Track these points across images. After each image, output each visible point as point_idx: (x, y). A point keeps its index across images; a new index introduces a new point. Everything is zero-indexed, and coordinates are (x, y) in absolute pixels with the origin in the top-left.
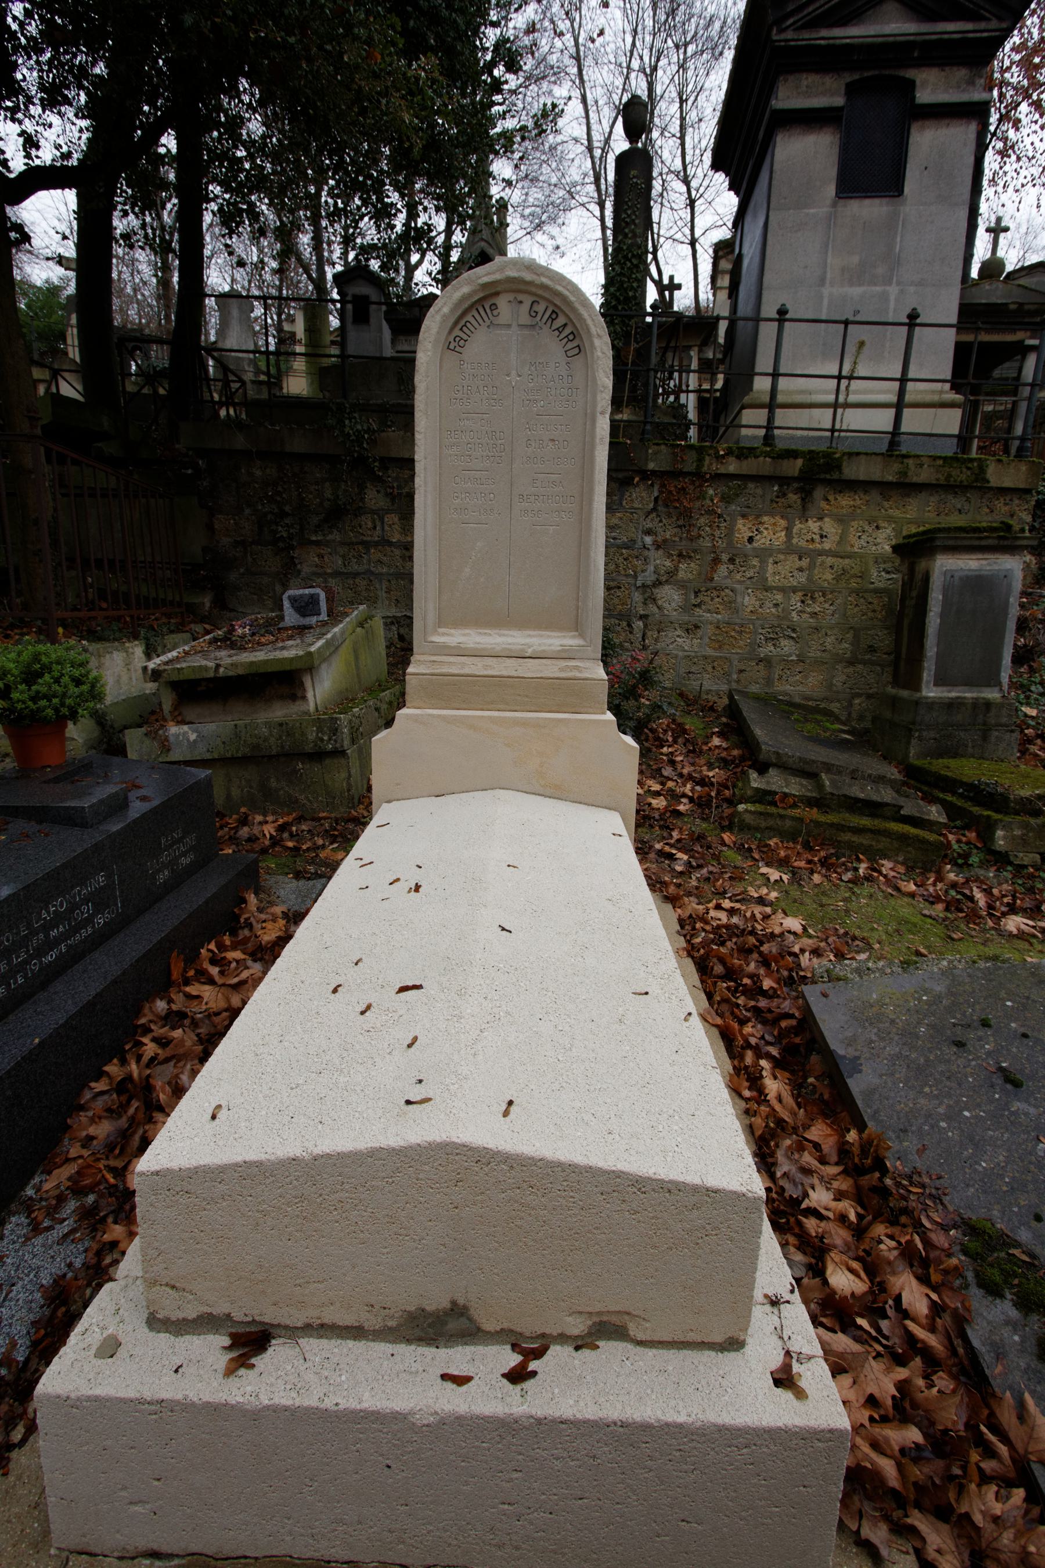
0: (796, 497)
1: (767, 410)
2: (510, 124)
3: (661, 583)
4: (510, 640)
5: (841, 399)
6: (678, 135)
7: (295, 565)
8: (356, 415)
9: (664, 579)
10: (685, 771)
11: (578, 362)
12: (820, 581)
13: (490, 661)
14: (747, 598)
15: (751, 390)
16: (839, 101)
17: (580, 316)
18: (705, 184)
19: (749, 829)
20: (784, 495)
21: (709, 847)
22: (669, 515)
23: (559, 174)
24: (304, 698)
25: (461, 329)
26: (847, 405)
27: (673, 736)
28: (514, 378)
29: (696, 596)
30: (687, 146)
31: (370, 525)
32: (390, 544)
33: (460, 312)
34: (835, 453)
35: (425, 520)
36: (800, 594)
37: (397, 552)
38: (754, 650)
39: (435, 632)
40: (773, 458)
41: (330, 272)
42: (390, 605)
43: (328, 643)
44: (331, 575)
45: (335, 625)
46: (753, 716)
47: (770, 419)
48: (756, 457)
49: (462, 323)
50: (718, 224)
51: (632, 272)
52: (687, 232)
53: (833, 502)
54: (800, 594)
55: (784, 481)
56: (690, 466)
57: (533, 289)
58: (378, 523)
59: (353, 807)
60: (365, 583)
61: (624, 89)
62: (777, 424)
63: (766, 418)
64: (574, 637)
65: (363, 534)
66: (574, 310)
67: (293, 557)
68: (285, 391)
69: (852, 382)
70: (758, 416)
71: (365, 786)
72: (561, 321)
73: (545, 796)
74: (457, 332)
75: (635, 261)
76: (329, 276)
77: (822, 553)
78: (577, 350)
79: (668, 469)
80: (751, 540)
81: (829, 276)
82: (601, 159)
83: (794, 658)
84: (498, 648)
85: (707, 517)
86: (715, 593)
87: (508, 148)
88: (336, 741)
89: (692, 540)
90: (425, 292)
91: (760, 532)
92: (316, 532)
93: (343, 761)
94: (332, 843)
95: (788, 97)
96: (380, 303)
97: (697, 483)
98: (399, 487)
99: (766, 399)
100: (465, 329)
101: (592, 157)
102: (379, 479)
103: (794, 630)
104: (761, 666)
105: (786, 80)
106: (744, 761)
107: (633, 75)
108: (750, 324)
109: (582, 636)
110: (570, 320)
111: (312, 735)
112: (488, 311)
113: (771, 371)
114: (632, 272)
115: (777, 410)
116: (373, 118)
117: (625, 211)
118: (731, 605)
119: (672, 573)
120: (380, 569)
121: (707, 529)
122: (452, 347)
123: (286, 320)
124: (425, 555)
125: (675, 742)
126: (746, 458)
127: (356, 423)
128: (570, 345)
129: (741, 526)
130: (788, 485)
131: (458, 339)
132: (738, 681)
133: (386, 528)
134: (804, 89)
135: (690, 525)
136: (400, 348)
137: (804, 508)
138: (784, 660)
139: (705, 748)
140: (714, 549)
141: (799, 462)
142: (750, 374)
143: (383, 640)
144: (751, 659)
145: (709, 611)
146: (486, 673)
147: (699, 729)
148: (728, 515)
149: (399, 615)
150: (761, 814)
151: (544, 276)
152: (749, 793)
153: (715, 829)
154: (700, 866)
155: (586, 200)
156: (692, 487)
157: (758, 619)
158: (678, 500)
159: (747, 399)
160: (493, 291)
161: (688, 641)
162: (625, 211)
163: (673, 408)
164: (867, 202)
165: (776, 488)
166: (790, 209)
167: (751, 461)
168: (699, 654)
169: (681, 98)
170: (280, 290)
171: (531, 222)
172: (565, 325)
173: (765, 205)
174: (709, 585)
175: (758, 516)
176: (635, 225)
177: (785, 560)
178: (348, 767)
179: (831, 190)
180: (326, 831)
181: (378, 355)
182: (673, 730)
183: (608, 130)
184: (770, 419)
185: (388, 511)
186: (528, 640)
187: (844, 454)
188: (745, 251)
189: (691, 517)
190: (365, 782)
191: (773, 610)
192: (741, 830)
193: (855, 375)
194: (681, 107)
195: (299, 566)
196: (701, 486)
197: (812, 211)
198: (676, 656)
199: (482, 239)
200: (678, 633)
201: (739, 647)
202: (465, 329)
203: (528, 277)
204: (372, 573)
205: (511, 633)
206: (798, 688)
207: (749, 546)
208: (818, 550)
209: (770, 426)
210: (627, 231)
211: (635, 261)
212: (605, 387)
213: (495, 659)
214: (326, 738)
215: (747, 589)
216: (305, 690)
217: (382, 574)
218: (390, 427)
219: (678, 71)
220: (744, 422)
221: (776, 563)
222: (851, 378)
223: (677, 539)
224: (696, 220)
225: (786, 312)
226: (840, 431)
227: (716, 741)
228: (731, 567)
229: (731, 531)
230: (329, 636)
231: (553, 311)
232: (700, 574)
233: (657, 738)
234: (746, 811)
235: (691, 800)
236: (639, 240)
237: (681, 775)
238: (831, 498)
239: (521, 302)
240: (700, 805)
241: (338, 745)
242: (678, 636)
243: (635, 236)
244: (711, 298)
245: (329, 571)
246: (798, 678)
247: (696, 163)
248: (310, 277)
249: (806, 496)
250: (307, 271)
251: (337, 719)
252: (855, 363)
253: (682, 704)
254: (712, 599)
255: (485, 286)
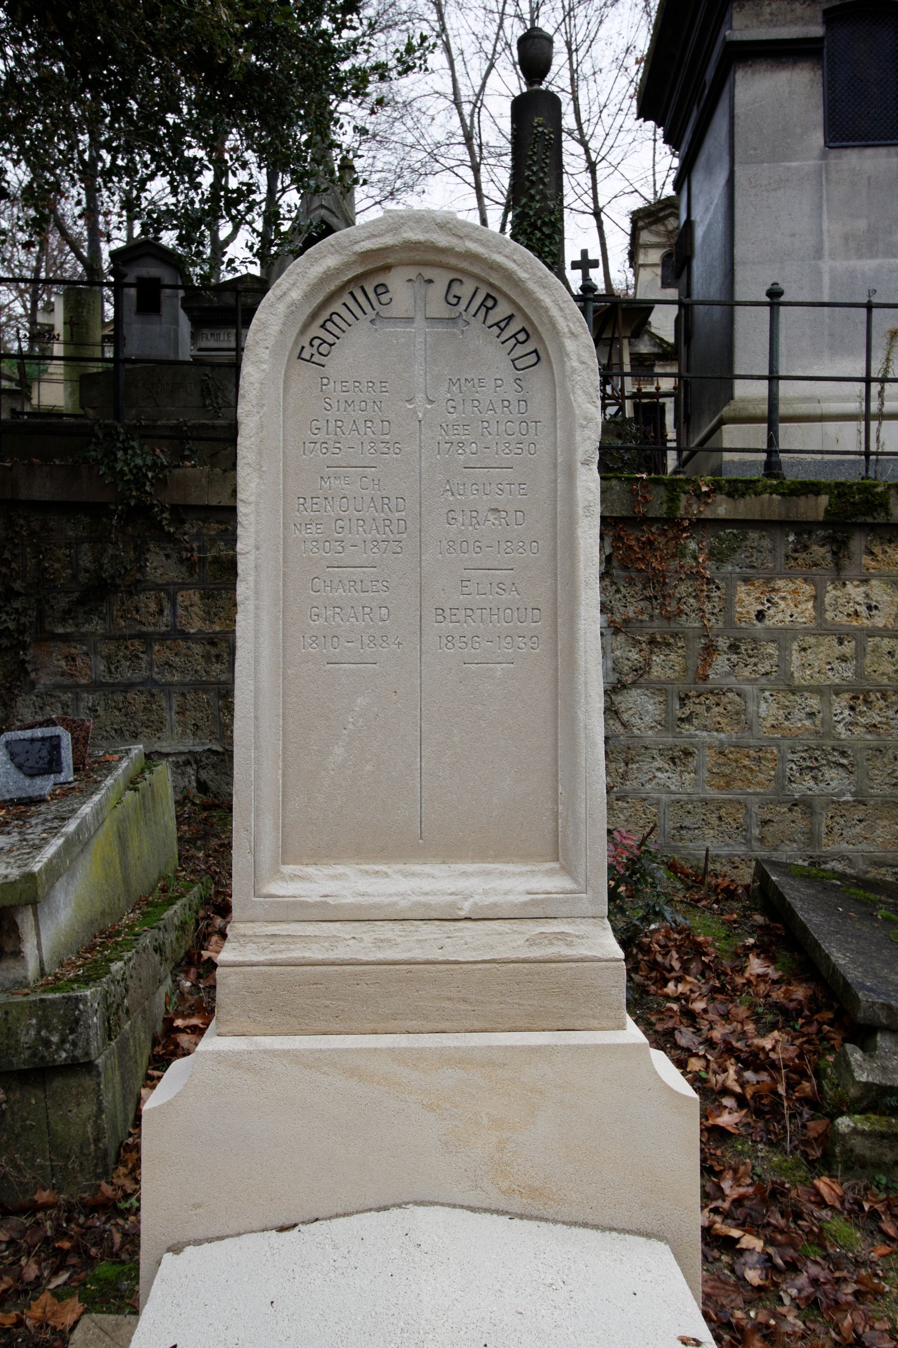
0: (823, 550)
1: (766, 425)
2: (360, 60)
3: (624, 687)
4: (426, 885)
5: (874, 407)
6: (569, 90)
7: (27, 673)
8: (135, 444)
9: (629, 679)
10: (717, 1034)
11: (536, 378)
12: (875, 676)
13: (388, 930)
14: (763, 705)
15: (732, 397)
16: (817, 30)
17: (537, 303)
18: (609, 142)
19: (863, 1166)
20: (806, 548)
21: (798, 1215)
22: (631, 583)
23: (417, 134)
24: (17, 954)
25: (323, 326)
26: (882, 417)
27: (680, 959)
28: (420, 405)
29: (683, 705)
30: (581, 101)
31: (153, 607)
32: (186, 636)
33: (320, 298)
34: (876, 486)
35: (257, 661)
36: (847, 696)
37: (197, 649)
38: (783, 788)
39: (276, 874)
40: (783, 495)
41: (106, 249)
42: (184, 733)
43: (69, 843)
44: (87, 688)
45: (86, 794)
46: (817, 920)
47: (772, 439)
48: (757, 494)
49: (325, 315)
50: (626, 191)
51: (544, 245)
52: (588, 200)
53: (881, 557)
54: (847, 696)
55: (803, 528)
56: (657, 507)
57: (453, 261)
58: (167, 605)
59: (106, 1174)
60: (143, 698)
61: (497, 39)
62: (782, 446)
63: (765, 439)
64: (550, 873)
65: (141, 622)
66: (527, 293)
67: (23, 662)
68: (35, 402)
69: (887, 386)
70: (757, 435)
71: (131, 1116)
72: (502, 310)
73: (513, 1216)
74: (315, 330)
75: (547, 230)
76: (105, 256)
77: (872, 633)
78: (533, 359)
79: (625, 513)
80: (760, 615)
81: (827, 245)
82: (472, 116)
83: (848, 798)
84: (403, 903)
85: (689, 583)
86: (712, 699)
87: (360, 92)
88: (74, 1044)
89: (669, 619)
90: (244, 272)
91: (775, 604)
92: (63, 621)
93: (88, 1082)
94: (55, 1273)
95: (747, 27)
96: (175, 287)
97: (671, 534)
98: (201, 549)
99: (764, 408)
100: (329, 325)
101: (461, 114)
102: (170, 537)
103: (843, 754)
104: (797, 814)
105: (742, 7)
106: (818, 1011)
107: (507, 22)
108: (717, 310)
109: (568, 870)
110: (519, 309)
111: (27, 1037)
112: (372, 296)
113: (766, 373)
114: (544, 245)
115: (781, 426)
116: (168, 22)
117: (529, 168)
118: (738, 716)
119: (642, 670)
120: (169, 677)
121: (692, 601)
122: (306, 355)
123: (43, 309)
124: (257, 727)
125: (686, 969)
126: (743, 495)
127: (135, 455)
128: (520, 350)
129: (743, 596)
130: (810, 533)
131: (317, 342)
132: (762, 840)
133: (180, 611)
134: (768, 17)
135: (664, 597)
136: (204, 344)
137: (838, 567)
138: (833, 802)
139: (740, 980)
140: (705, 632)
141: (824, 500)
142: (728, 378)
143: (170, 791)
144: (781, 803)
145: (705, 728)
146: (380, 956)
147: (718, 939)
148: (722, 580)
149: (199, 749)
150: (882, 1136)
151: (471, 239)
152: (853, 1092)
153: (797, 1167)
154: (793, 1267)
155: (453, 163)
156: (662, 540)
157: (784, 737)
158: (643, 559)
159: (726, 411)
160: (380, 264)
161: (675, 777)
162: (529, 168)
163: (616, 423)
164: (869, 152)
165: (791, 538)
166: (763, 162)
167: (750, 499)
168: (694, 797)
169: (569, 49)
170: (37, 270)
171: (381, 190)
172: (510, 318)
173: (726, 159)
174: (702, 686)
175: (768, 581)
176: (544, 184)
177: (818, 645)
178: (98, 1093)
179: (818, 138)
180: (47, 1240)
181: (172, 357)
182: (679, 949)
183: (480, 82)
184: (772, 439)
185: (184, 586)
186: (462, 884)
187: (890, 487)
188: (696, 216)
189: (665, 584)
190: (131, 1107)
191: (807, 723)
192: (848, 1169)
193: (890, 376)
194: (570, 59)
195: (33, 675)
196: (677, 537)
197: (794, 164)
198: (658, 803)
199: (322, 206)
200: (656, 764)
201: (758, 783)
202: (329, 325)
203: (443, 240)
204: (156, 683)
205: (427, 869)
206: (859, 847)
207: (759, 625)
208: (867, 629)
209: (772, 449)
210: (532, 192)
211: (547, 230)
212: (589, 419)
213: (397, 926)
214: (55, 1039)
215: (763, 690)
216: (19, 939)
217: (171, 684)
218: (188, 458)
219: (564, 20)
220: (726, 444)
221: (804, 649)
222: (883, 380)
223: (645, 617)
224: (599, 186)
225: (781, 293)
226: (876, 454)
227: (756, 966)
228: (734, 657)
229: (728, 603)
230: (71, 827)
231: (488, 296)
232: (685, 670)
233: (654, 965)
234: (855, 1131)
235: (741, 1102)
236: (551, 204)
237: (710, 1043)
238: (877, 550)
239: (430, 281)
240: (758, 1113)
241: (78, 1052)
242: (659, 769)
243: (545, 198)
244: (631, 280)
245: (83, 681)
246: (858, 829)
247: (594, 120)
248: (79, 256)
249: (839, 548)
250: (75, 249)
251: (78, 1000)
252: (888, 360)
253: (679, 886)
254: (708, 709)
255: (366, 255)
